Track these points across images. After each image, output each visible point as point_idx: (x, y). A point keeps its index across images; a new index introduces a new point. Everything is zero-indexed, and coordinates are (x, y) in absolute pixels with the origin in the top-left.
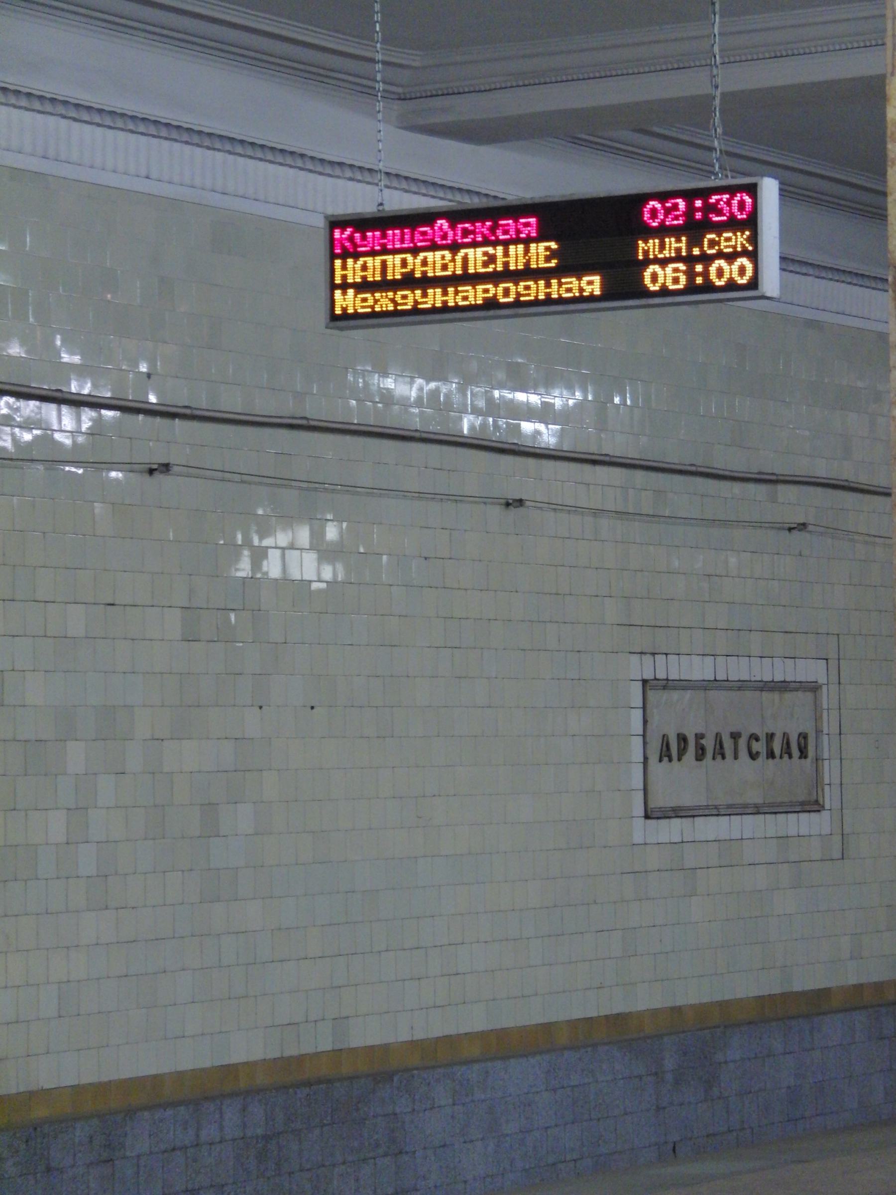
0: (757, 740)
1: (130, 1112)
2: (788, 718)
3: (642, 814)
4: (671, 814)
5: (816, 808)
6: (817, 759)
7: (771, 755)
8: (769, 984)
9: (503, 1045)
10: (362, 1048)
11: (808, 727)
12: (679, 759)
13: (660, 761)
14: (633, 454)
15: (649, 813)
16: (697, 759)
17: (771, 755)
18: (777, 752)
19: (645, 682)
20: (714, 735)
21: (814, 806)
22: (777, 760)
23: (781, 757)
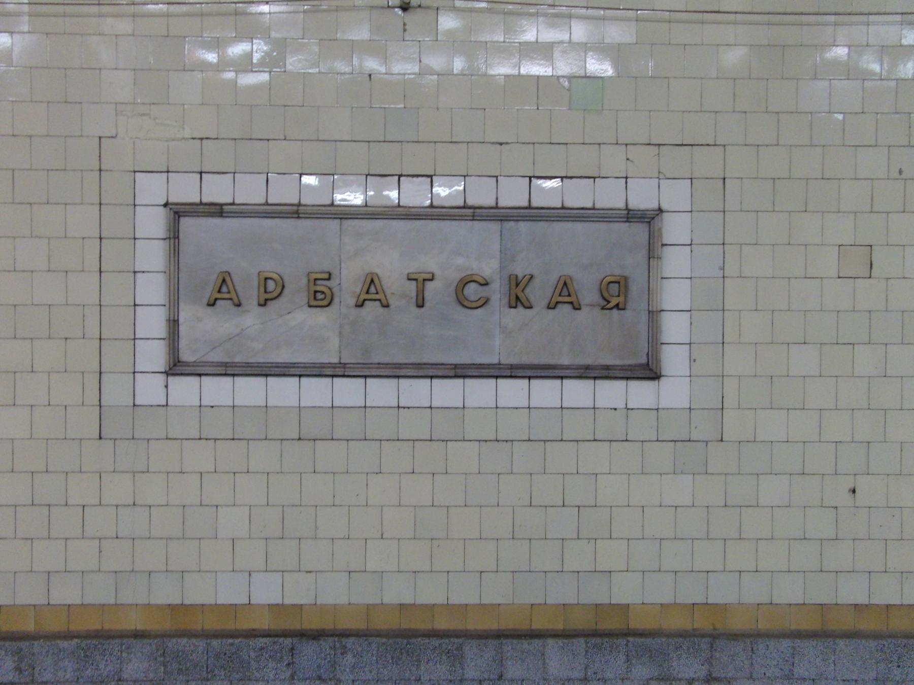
2: (580, 254)
6: (654, 315)
7: (517, 301)
11: (631, 264)
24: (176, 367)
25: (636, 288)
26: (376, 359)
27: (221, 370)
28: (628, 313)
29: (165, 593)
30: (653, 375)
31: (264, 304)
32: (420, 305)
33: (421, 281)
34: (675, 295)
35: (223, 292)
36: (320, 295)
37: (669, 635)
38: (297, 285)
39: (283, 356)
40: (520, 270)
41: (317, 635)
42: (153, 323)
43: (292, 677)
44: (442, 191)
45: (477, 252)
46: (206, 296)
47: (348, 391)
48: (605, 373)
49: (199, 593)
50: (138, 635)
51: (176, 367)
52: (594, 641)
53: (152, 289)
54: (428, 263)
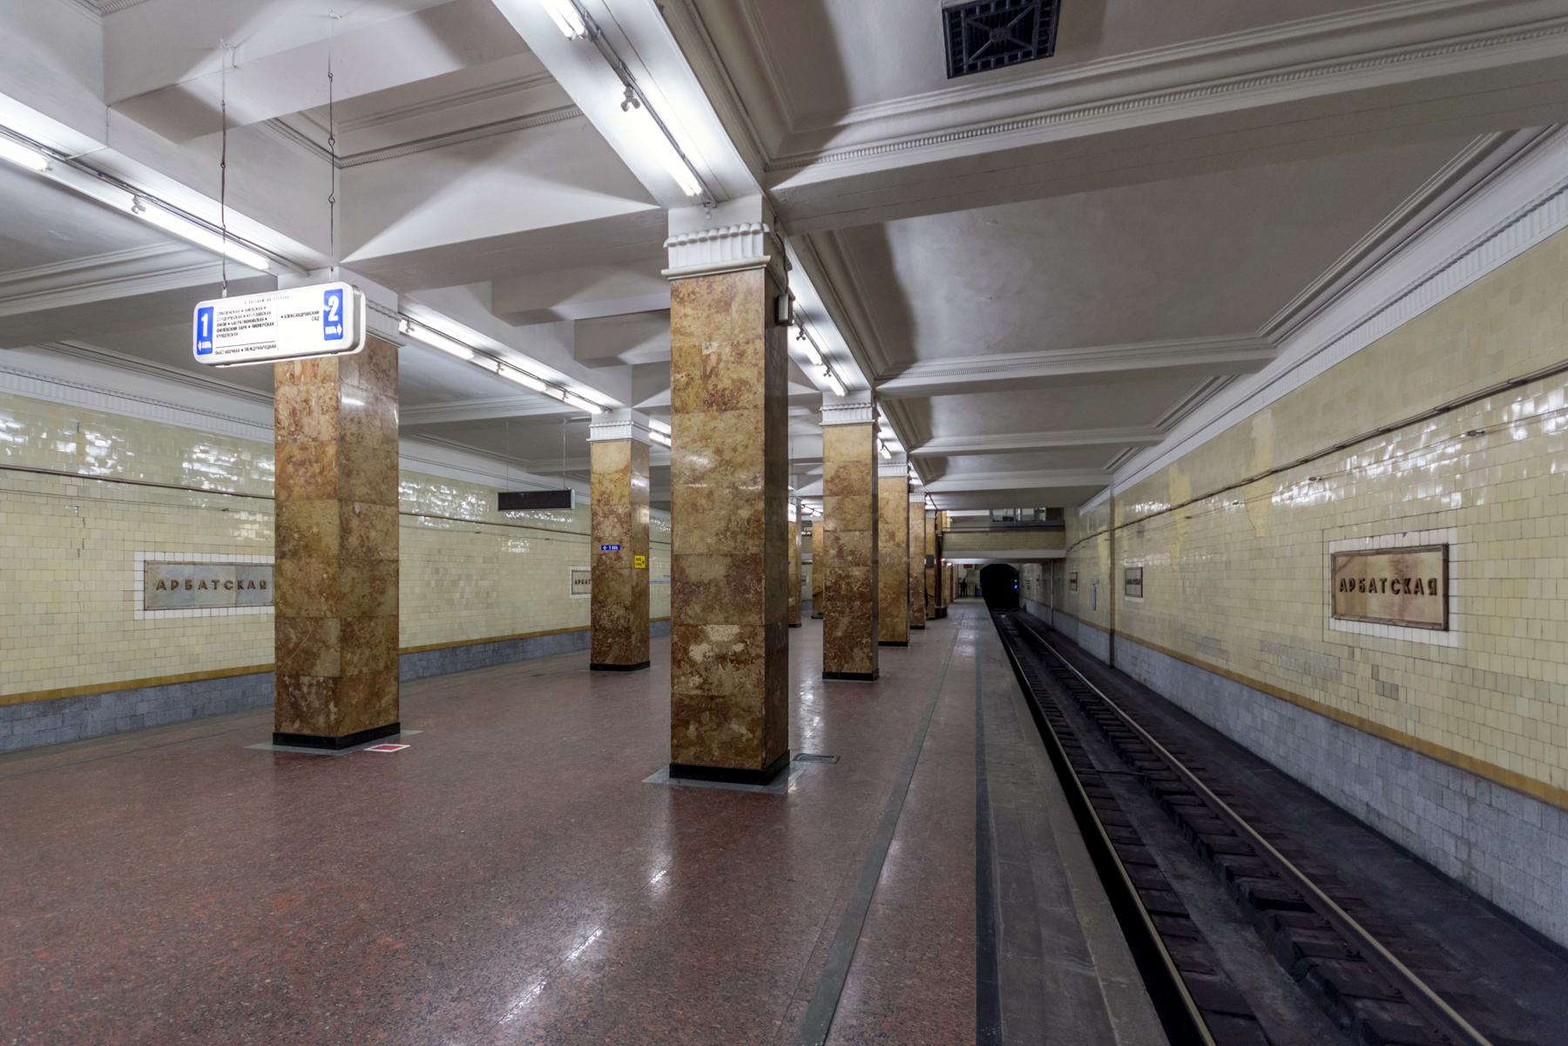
9: (545, 634)
33: (1384, 581)
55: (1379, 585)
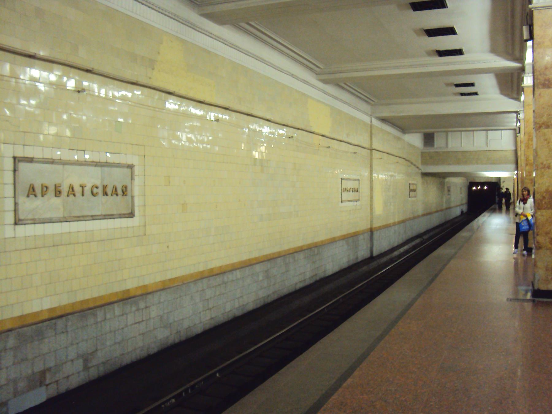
0: (97, 187)
1: (360, 234)
2: (117, 178)
3: (12, 221)
4: (122, 216)
5: (131, 216)
6: (133, 197)
7: (105, 194)
8: (329, 237)
10: (120, 292)
11: (127, 182)
12: (42, 196)
13: (28, 196)
14: (397, 155)
15: (17, 222)
16: (56, 196)
17: (105, 194)
18: (109, 193)
19: (15, 158)
20: (112, 187)
21: (131, 215)
22: (120, 196)
23: (112, 195)
24: (17, 222)
25: (129, 188)
26: (73, 215)
27: (103, 217)
28: (127, 197)
29: (17, 313)
30: (44, 193)
31: (42, 196)
32: (83, 195)
34: (137, 191)
35: (32, 191)
36: (58, 193)
37: (138, 296)
38: (52, 189)
39: (48, 215)
40: (105, 184)
41: (61, 317)
42: (9, 204)
43: (56, 334)
44: (87, 157)
45: (92, 178)
46: (26, 195)
47: (66, 227)
48: (78, 219)
49: (27, 310)
50: (10, 330)
51: (17, 222)
52: (124, 302)
53: (9, 190)
54: (84, 181)
55: (78, 189)
